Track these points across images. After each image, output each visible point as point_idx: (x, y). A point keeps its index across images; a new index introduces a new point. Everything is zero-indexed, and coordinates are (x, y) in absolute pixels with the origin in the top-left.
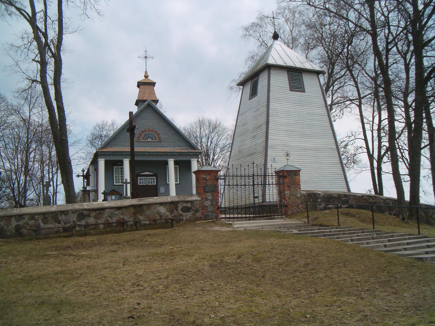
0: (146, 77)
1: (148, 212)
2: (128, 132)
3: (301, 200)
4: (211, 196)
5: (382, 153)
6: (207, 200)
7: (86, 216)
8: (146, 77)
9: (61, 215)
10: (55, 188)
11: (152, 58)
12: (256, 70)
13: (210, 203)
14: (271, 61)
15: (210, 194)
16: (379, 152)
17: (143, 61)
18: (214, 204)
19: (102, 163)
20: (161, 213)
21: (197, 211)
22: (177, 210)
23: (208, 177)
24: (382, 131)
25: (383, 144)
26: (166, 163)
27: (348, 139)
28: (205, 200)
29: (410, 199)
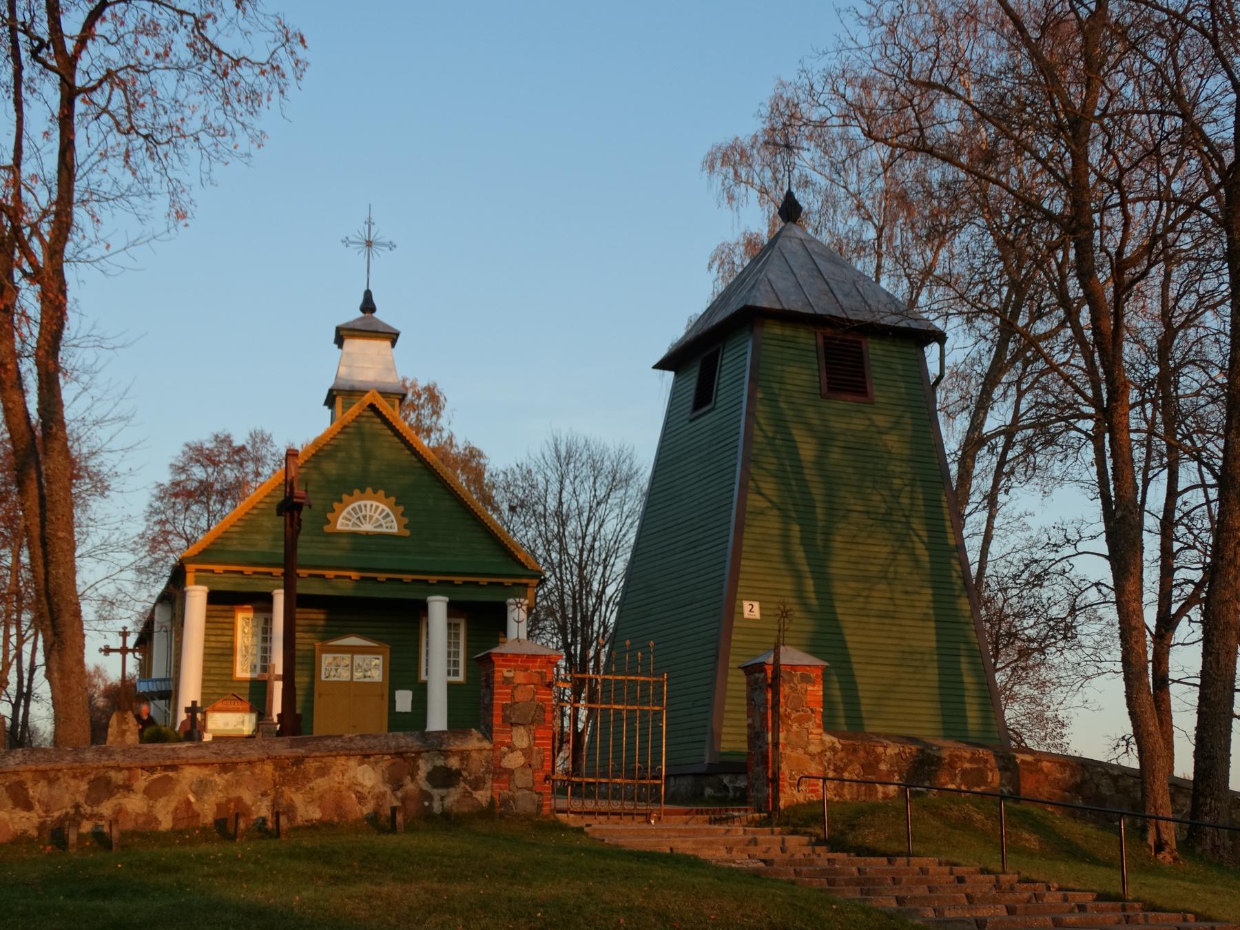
0: (368, 306)
1: (319, 781)
2: (279, 514)
3: (821, 763)
4: (526, 739)
5: (1174, 609)
6: (512, 748)
7: (118, 787)
8: (368, 306)
9: (36, 782)
10: (26, 675)
11: (391, 246)
12: (706, 327)
13: (522, 761)
14: (764, 300)
15: (522, 730)
16: (1165, 599)
17: (356, 256)
18: (533, 762)
19: (197, 598)
20: (360, 785)
21: (477, 784)
22: (413, 779)
23: (520, 677)
24: (1181, 530)
25: (1179, 575)
26: (421, 609)
27: (1052, 556)
28: (505, 749)
29: (1196, 773)
